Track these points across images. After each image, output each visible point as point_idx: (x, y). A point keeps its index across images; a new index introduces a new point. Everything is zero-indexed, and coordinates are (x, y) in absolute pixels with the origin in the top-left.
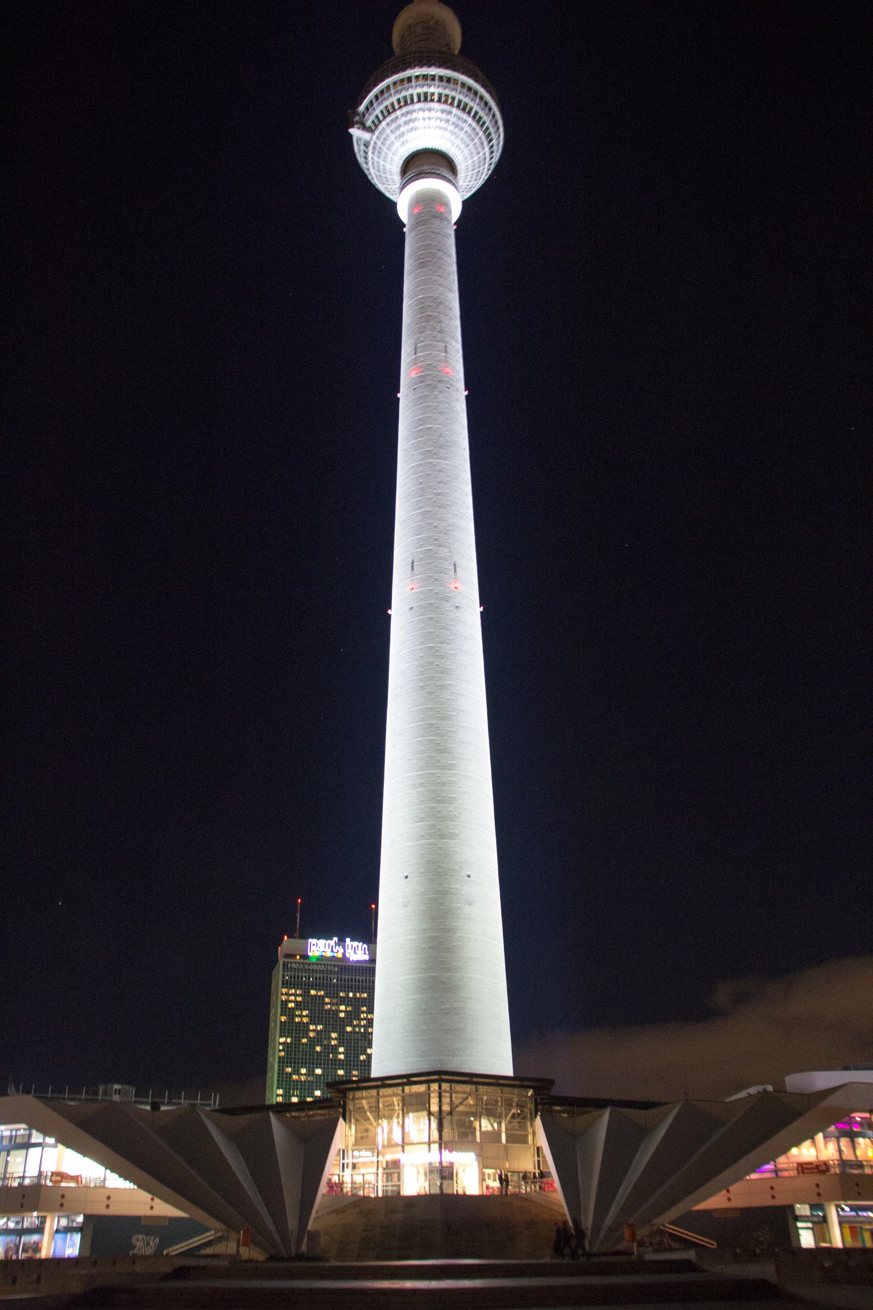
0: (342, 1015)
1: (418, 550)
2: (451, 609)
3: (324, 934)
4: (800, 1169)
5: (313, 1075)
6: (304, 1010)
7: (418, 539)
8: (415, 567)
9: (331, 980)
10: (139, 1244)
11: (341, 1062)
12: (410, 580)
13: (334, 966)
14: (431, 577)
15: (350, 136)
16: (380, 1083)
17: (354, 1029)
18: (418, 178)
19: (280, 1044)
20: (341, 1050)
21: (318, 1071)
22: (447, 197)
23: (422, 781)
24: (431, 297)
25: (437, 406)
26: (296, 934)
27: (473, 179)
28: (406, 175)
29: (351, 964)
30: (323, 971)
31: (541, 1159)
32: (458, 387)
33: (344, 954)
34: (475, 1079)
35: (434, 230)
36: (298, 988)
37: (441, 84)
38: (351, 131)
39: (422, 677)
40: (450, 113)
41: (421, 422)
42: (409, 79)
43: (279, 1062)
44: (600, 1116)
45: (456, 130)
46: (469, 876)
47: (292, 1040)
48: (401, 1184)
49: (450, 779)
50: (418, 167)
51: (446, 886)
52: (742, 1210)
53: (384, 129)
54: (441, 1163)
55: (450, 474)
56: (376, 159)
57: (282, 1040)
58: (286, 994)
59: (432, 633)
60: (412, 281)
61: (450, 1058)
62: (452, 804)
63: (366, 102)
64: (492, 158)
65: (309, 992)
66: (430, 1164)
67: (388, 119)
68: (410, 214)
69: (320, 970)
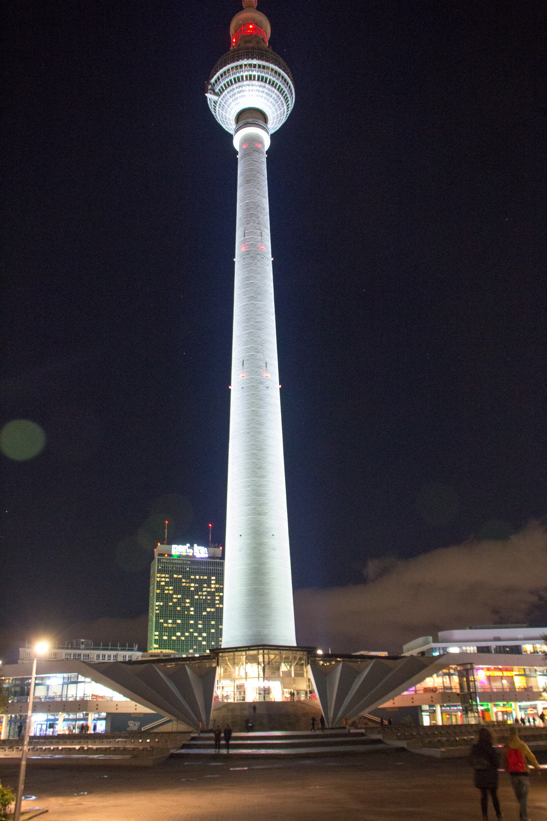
0: (192, 589)
1: (246, 354)
2: (264, 389)
4: (425, 691)
5: (176, 624)
6: (170, 586)
7: (246, 348)
8: (244, 364)
9: (186, 568)
10: (131, 725)
11: (192, 616)
12: (241, 371)
13: (188, 560)
14: (253, 370)
15: (206, 97)
16: (235, 650)
17: (199, 597)
18: (246, 126)
19: (157, 606)
20: (192, 609)
21: (179, 621)
22: (262, 138)
23: (249, 484)
24: (253, 202)
25: (257, 269)
26: (165, 541)
27: (277, 123)
28: (239, 124)
30: (181, 563)
31: (310, 684)
32: (268, 257)
33: (193, 553)
34: (280, 648)
35: (255, 160)
36: (166, 574)
37: (259, 69)
38: (207, 95)
39: (248, 427)
40: (265, 87)
41: (248, 279)
42: (241, 66)
43: (156, 616)
46: (273, 535)
47: (163, 604)
48: (245, 696)
49: (263, 483)
51: (262, 540)
52: (400, 708)
53: (226, 95)
55: (263, 310)
56: (221, 111)
57: (158, 604)
58: (160, 577)
59: (254, 402)
60: (242, 191)
61: (264, 629)
62: (264, 497)
63: (215, 77)
64: (288, 111)
65: (173, 576)
66: (259, 687)
67: (228, 90)
68: (241, 147)
69: (179, 563)
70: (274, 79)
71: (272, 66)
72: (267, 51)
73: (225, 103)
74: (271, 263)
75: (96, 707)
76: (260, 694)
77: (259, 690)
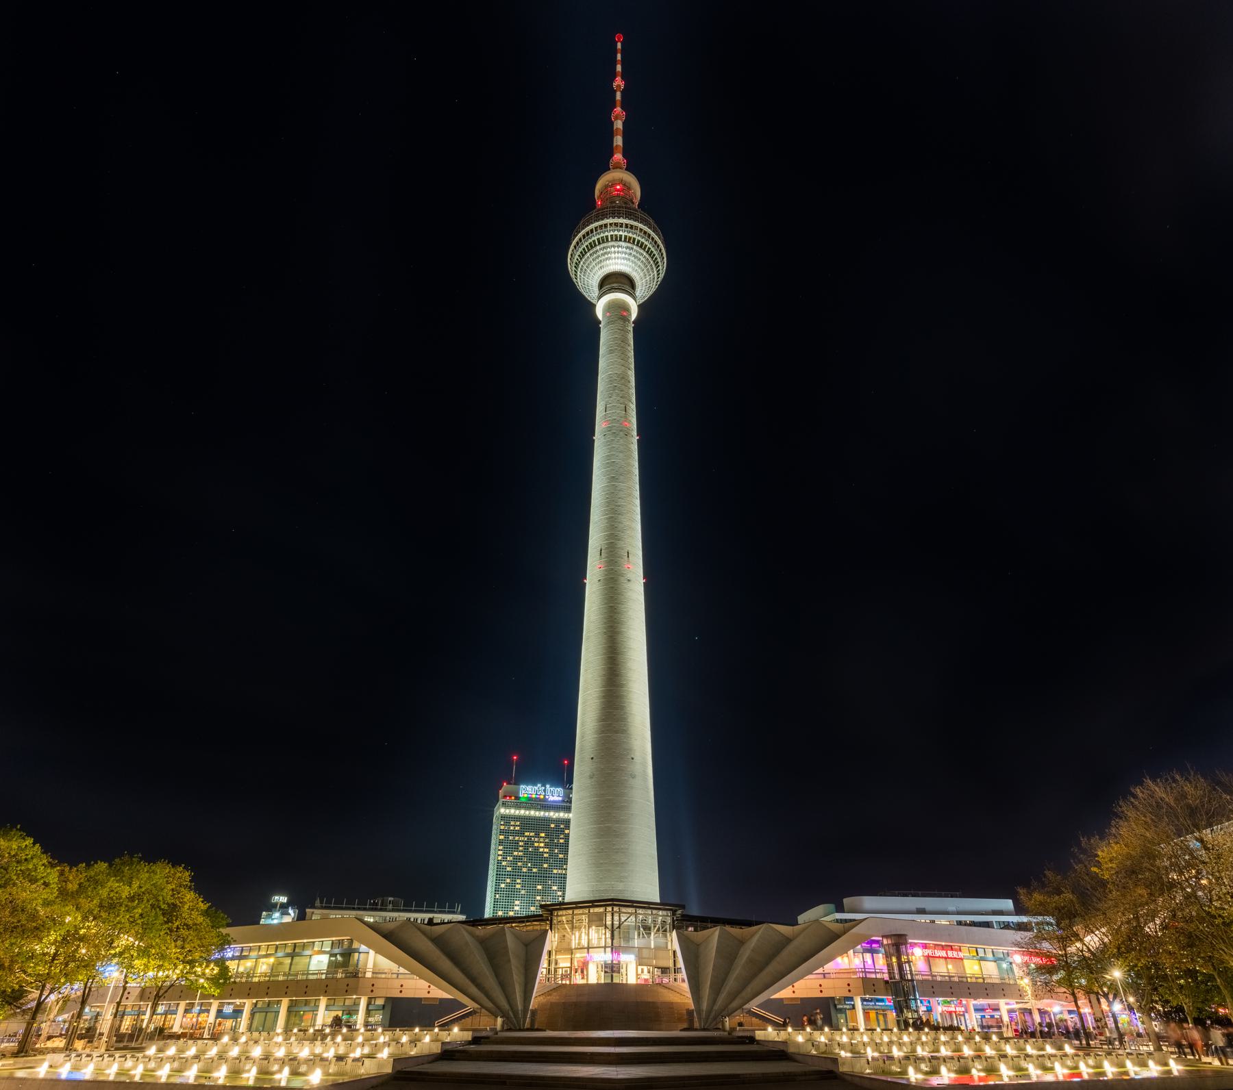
3: (533, 782)
8: (602, 555)
29: (549, 804)
37: (626, 229)
40: (632, 249)
42: (606, 226)
44: (713, 934)
45: (636, 260)
50: (610, 284)
53: (588, 257)
54: (612, 961)
68: (604, 315)
70: (643, 240)
71: (641, 226)
72: (637, 211)
73: (587, 267)
74: (636, 441)
75: (305, 989)
76: (606, 972)
77: (606, 967)
